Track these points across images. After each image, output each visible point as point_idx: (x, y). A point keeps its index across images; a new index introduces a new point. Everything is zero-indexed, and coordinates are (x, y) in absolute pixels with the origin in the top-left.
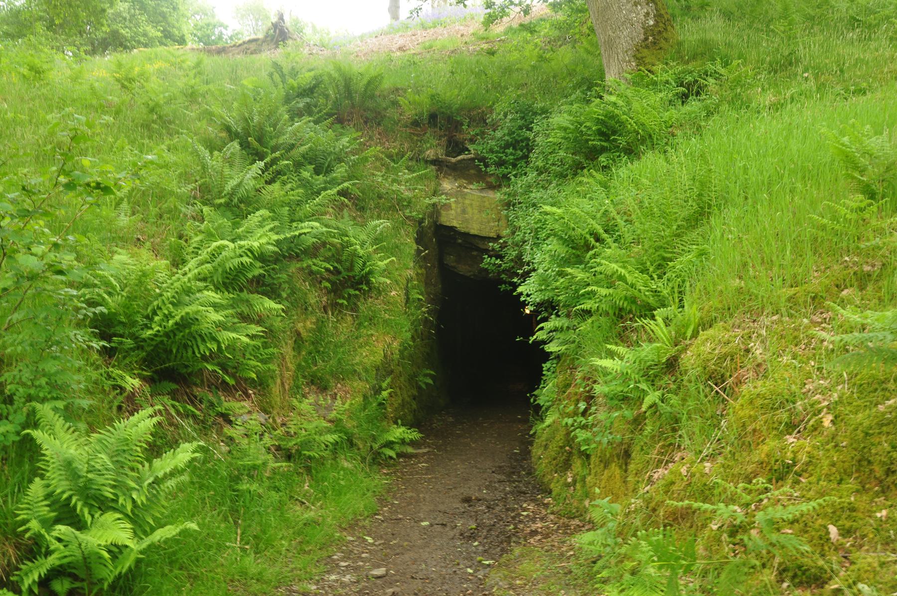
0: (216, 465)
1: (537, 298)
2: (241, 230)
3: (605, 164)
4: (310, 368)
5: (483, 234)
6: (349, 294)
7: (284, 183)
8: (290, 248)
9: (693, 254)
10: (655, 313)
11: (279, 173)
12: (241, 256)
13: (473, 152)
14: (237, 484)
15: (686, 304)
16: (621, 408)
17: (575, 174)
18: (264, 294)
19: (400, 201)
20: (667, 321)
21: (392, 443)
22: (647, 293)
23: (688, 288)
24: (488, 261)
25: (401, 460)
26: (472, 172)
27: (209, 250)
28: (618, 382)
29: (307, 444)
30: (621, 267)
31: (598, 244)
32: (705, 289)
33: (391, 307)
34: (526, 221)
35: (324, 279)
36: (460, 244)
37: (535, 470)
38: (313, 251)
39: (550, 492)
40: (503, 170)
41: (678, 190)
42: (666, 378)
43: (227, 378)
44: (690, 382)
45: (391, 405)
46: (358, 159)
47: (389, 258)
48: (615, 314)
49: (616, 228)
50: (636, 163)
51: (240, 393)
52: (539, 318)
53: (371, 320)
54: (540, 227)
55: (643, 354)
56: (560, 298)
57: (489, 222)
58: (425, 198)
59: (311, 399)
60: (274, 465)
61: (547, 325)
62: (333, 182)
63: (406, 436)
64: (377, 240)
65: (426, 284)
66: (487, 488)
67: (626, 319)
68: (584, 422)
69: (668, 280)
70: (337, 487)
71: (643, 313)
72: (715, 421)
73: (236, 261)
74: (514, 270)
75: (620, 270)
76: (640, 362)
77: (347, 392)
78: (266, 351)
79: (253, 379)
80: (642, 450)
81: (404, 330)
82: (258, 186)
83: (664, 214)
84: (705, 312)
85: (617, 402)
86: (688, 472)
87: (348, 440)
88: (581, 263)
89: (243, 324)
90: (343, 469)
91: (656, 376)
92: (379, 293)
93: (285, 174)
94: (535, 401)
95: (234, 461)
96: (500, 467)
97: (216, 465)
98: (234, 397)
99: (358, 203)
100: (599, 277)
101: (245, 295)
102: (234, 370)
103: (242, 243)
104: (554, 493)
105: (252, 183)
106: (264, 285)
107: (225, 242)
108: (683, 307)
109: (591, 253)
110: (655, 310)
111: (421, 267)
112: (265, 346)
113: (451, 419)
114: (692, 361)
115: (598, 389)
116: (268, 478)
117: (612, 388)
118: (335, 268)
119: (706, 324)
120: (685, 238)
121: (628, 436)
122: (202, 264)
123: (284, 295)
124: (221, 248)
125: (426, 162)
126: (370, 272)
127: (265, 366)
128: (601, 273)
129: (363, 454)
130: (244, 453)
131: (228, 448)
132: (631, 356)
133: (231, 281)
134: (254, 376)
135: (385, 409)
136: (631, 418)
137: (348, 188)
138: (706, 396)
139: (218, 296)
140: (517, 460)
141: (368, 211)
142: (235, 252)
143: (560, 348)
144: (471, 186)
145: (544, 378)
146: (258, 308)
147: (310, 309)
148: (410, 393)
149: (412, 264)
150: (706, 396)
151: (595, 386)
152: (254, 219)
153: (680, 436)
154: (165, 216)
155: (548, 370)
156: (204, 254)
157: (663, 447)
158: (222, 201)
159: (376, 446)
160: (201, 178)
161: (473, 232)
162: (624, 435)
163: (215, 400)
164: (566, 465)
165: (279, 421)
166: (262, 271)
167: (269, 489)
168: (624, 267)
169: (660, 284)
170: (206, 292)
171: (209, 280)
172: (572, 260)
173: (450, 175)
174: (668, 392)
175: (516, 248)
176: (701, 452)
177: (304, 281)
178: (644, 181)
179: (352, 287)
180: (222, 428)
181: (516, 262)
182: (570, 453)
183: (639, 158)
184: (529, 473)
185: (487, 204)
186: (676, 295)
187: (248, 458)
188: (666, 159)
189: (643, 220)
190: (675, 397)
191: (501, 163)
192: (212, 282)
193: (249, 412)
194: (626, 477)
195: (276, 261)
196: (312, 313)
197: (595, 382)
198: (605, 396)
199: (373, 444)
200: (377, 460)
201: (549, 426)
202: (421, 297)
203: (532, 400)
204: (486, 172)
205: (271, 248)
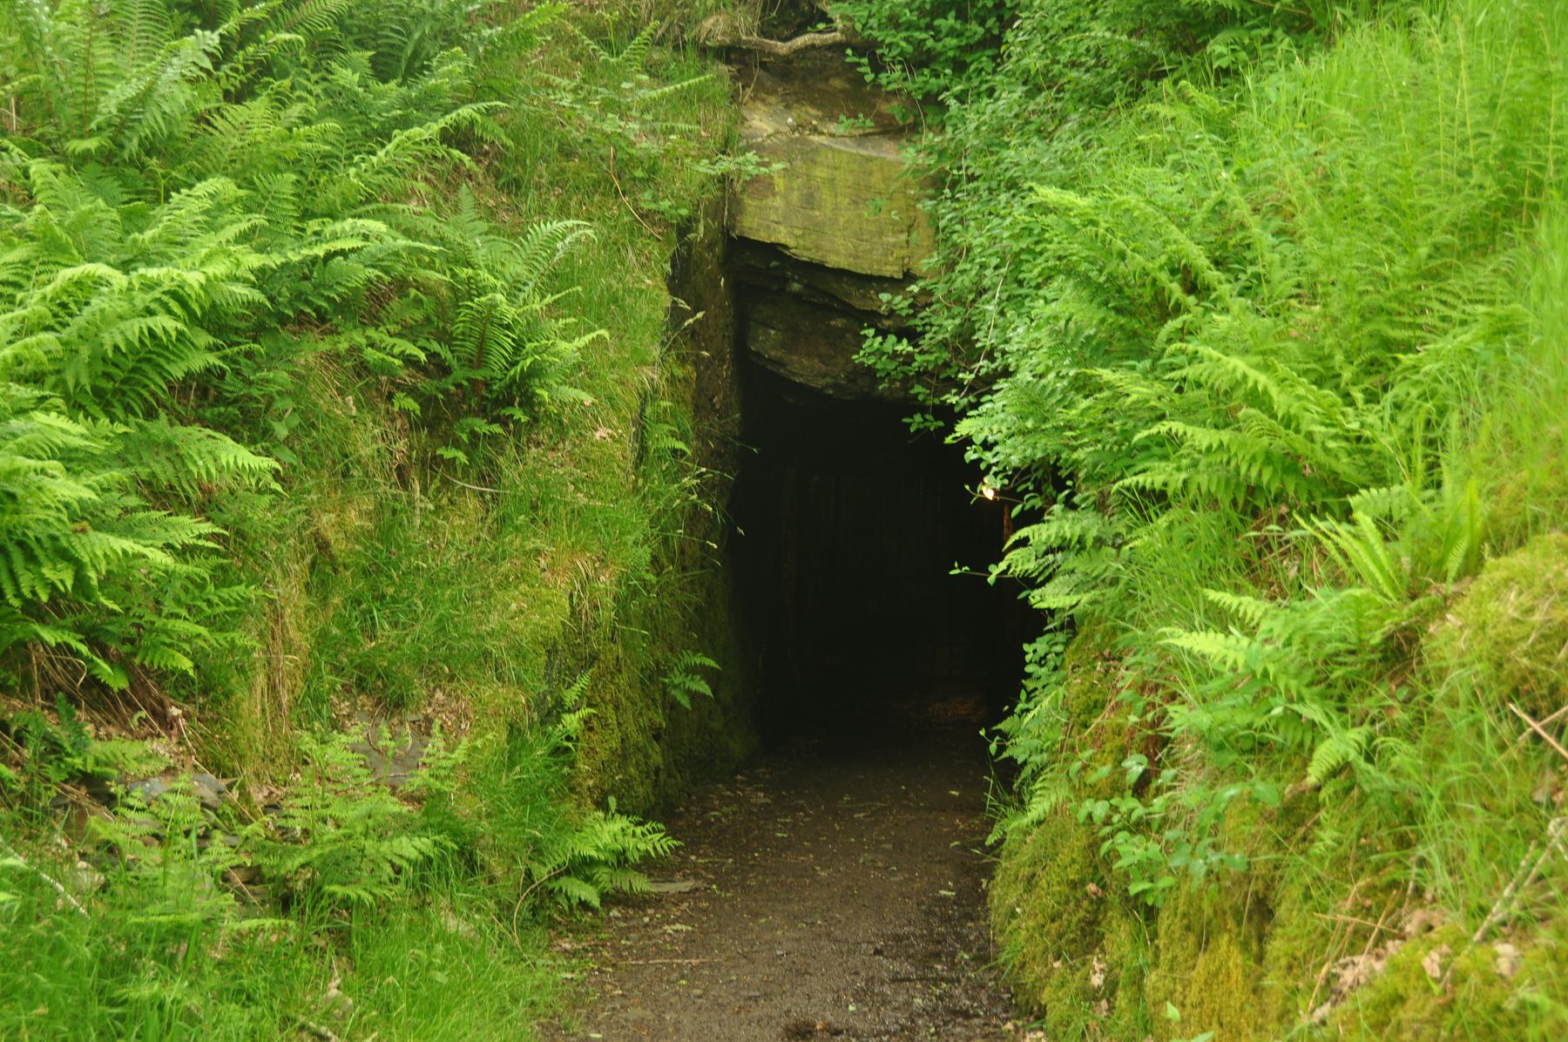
0: (59, 926)
1: (1013, 454)
2: (149, 234)
3: (1224, 63)
4: (355, 643)
5: (864, 268)
6: (473, 434)
7: (281, 101)
8: (299, 296)
9: (1475, 329)
10: (1353, 501)
11: (266, 68)
12: (150, 312)
13: (839, 24)
14: (123, 982)
15: (1447, 479)
16: (1247, 774)
17: (1136, 94)
18: (224, 426)
19: (625, 165)
20: (1388, 526)
21: (590, 862)
22: (1332, 444)
23: (1454, 431)
24: (874, 348)
25: (615, 913)
26: (837, 83)
27: (49, 289)
28: (1240, 700)
29: (339, 864)
30: (1257, 367)
31: (1191, 300)
32: (1508, 432)
33: (594, 472)
34: (988, 231)
35: (399, 387)
36: (797, 297)
37: (999, 949)
38: (369, 306)
39: (1041, 1014)
40: (924, 80)
41: (1442, 138)
42: (1382, 693)
43: (104, 669)
44: (1453, 703)
45: (591, 752)
46: (502, 37)
47: (590, 330)
48: (1234, 503)
49: (1249, 255)
50: (1318, 60)
51: (144, 714)
52: (1015, 512)
53: (534, 508)
54: (1028, 251)
55: (1315, 619)
56: (1079, 455)
57: (881, 233)
58: (697, 159)
59: (356, 733)
60: (237, 926)
61: (1039, 534)
62: (429, 104)
63: (630, 843)
64: (555, 279)
65: (697, 409)
66: (859, 997)
67: (1267, 517)
68: (1140, 811)
69: (1397, 406)
70: (423, 991)
71: (1318, 503)
72: (1530, 823)
73: (135, 328)
74: (950, 372)
75: (1254, 374)
76: (1305, 643)
77: (461, 716)
78: (224, 592)
79: (184, 674)
80: (1307, 897)
81: (630, 539)
82: (201, 107)
83: (1394, 212)
84: (1505, 500)
85: (1233, 757)
86: (1443, 968)
87: (461, 853)
88: (1141, 354)
89: (155, 514)
90: (443, 936)
91: (1350, 685)
92: (562, 430)
93: (284, 74)
94: (1001, 749)
95: (117, 915)
96: (898, 938)
97: (59, 926)
98: (124, 725)
99: (497, 167)
100: (1192, 394)
101: (161, 427)
102: (127, 648)
103: (153, 273)
104: (1052, 1018)
105: (184, 94)
106: (220, 400)
107: (100, 269)
108: (1439, 485)
109: (1173, 324)
110: (1354, 492)
111: (682, 360)
112: (223, 577)
113: (761, 798)
114: (1461, 645)
115: (1181, 718)
116: (219, 964)
117: (1221, 715)
118: (432, 355)
119: (1504, 537)
120: (1454, 283)
121: (1266, 856)
122: (31, 333)
123: (281, 431)
124: (86, 288)
125: (703, 51)
126: (535, 372)
127: (220, 636)
128: (1199, 385)
129: (505, 897)
130: (149, 891)
131: (99, 878)
132: (1277, 626)
133: (116, 384)
134: (186, 664)
135: (572, 765)
136: (1274, 804)
137: (472, 123)
138: (1502, 747)
139: (80, 429)
140: (946, 920)
141: (533, 193)
142: (131, 301)
143: (1074, 599)
144: (832, 127)
145: (1030, 684)
146: (200, 466)
147: (356, 473)
148: (644, 721)
149: (656, 352)
150: (1502, 747)
151: (1170, 708)
152: (190, 204)
153: (1422, 863)
154: (1321, 941)
155: (1041, 662)
156: (34, 302)
157: (1371, 890)
158: (92, 144)
159: (542, 873)
160: (22, 70)
161: (833, 261)
162: (1252, 854)
163: (63, 735)
164: (1089, 937)
165: (259, 797)
166: (213, 359)
167: (220, 995)
168: (1266, 368)
169: (1371, 419)
170: (39, 417)
171: (51, 380)
172: (1116, 346)
173: (773, 92)
174: (1385, 731)
175: (957, 309)
176: (1483, 911)
177: (341, 393)
178: (1340, 113)
179: (482, 412)
180: (82, 816)
181: (956, 351)
182: (1099, 904)
183: (1329, 44)
184: (982, 958)
185: (875, 180)
186: (1418, 450)
187: (158, 907)
188: (1412, 45)
189: (1329, 230)
190: (1405, 746)
191: (920, 60)
192: (60, 385)
193: (170, 771)
194: (1260, 978)
195: (258, 332)
196: (362, 485)
197: (1173, 697)
198: (1203, 738)
199: (535, 866)
200: (543, 910)
201: (1040, 823)
202: (680, 445)
203: (993, 748)
204: (877, 86)
205: (240, 290)
